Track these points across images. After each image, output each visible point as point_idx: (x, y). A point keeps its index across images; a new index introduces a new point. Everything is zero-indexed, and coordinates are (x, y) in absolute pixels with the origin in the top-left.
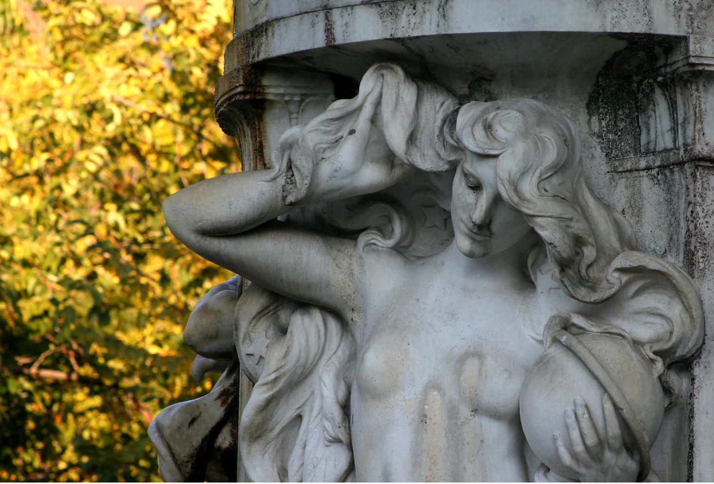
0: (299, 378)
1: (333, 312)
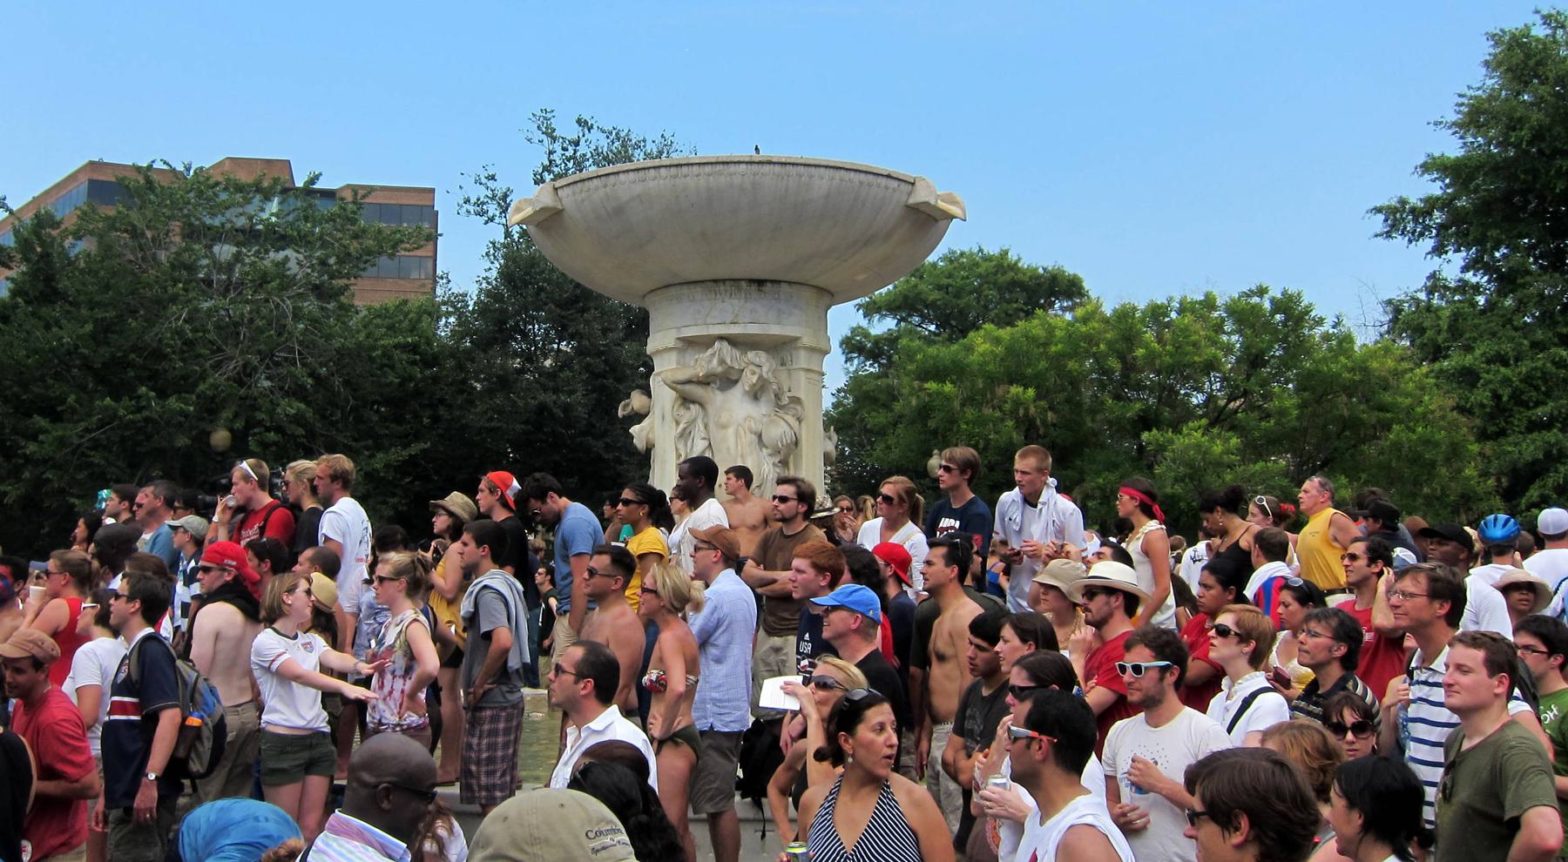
0: (692, 422)
1: (701, 405)
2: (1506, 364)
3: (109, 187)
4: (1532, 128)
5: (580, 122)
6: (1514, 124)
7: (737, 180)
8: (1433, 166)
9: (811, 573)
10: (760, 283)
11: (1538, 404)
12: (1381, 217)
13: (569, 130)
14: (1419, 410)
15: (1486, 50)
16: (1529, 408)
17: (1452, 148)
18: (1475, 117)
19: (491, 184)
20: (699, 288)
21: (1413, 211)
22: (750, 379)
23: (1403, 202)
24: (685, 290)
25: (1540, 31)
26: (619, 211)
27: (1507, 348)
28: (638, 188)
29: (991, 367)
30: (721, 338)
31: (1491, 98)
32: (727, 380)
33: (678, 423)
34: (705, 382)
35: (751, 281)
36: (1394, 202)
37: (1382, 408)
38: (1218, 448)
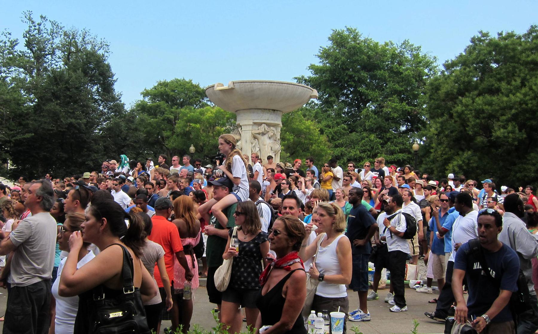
2: (330, 128)
3: (177, 81)
4: (342, 61)
5: (42, 17)
6: (336, 59)
7: (284, 87)
8: (312, 67)
9: (389, 180)
10: (274, 110)
11: (338, 139)
12: (296, 80)
13: (37, 20)
14: (319, 141)
15: (330, 33)
16: (335, 141)
17: (318, 63)
18: (326, 55)
19: (9, 36)
20: (260, 111)
21: (305, 80)
22: (271, 134)
23: (303, 77)
24: (256, 110)
25: (346, 33)
26: (253, 91)
27: (330, 123)
28: (260, 86)
29: (211, 121)
30: (264, 123)
31: (329, 50)
32: (263, 134)
33: (252, 143)
34: (259, 134)
35: (273, 110)
36: (300, 77)
37: (310, 140)
38: (329, 151)
